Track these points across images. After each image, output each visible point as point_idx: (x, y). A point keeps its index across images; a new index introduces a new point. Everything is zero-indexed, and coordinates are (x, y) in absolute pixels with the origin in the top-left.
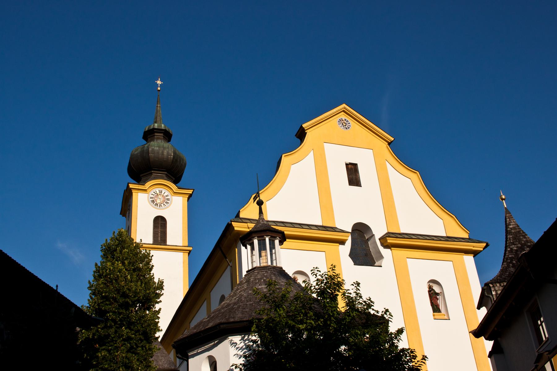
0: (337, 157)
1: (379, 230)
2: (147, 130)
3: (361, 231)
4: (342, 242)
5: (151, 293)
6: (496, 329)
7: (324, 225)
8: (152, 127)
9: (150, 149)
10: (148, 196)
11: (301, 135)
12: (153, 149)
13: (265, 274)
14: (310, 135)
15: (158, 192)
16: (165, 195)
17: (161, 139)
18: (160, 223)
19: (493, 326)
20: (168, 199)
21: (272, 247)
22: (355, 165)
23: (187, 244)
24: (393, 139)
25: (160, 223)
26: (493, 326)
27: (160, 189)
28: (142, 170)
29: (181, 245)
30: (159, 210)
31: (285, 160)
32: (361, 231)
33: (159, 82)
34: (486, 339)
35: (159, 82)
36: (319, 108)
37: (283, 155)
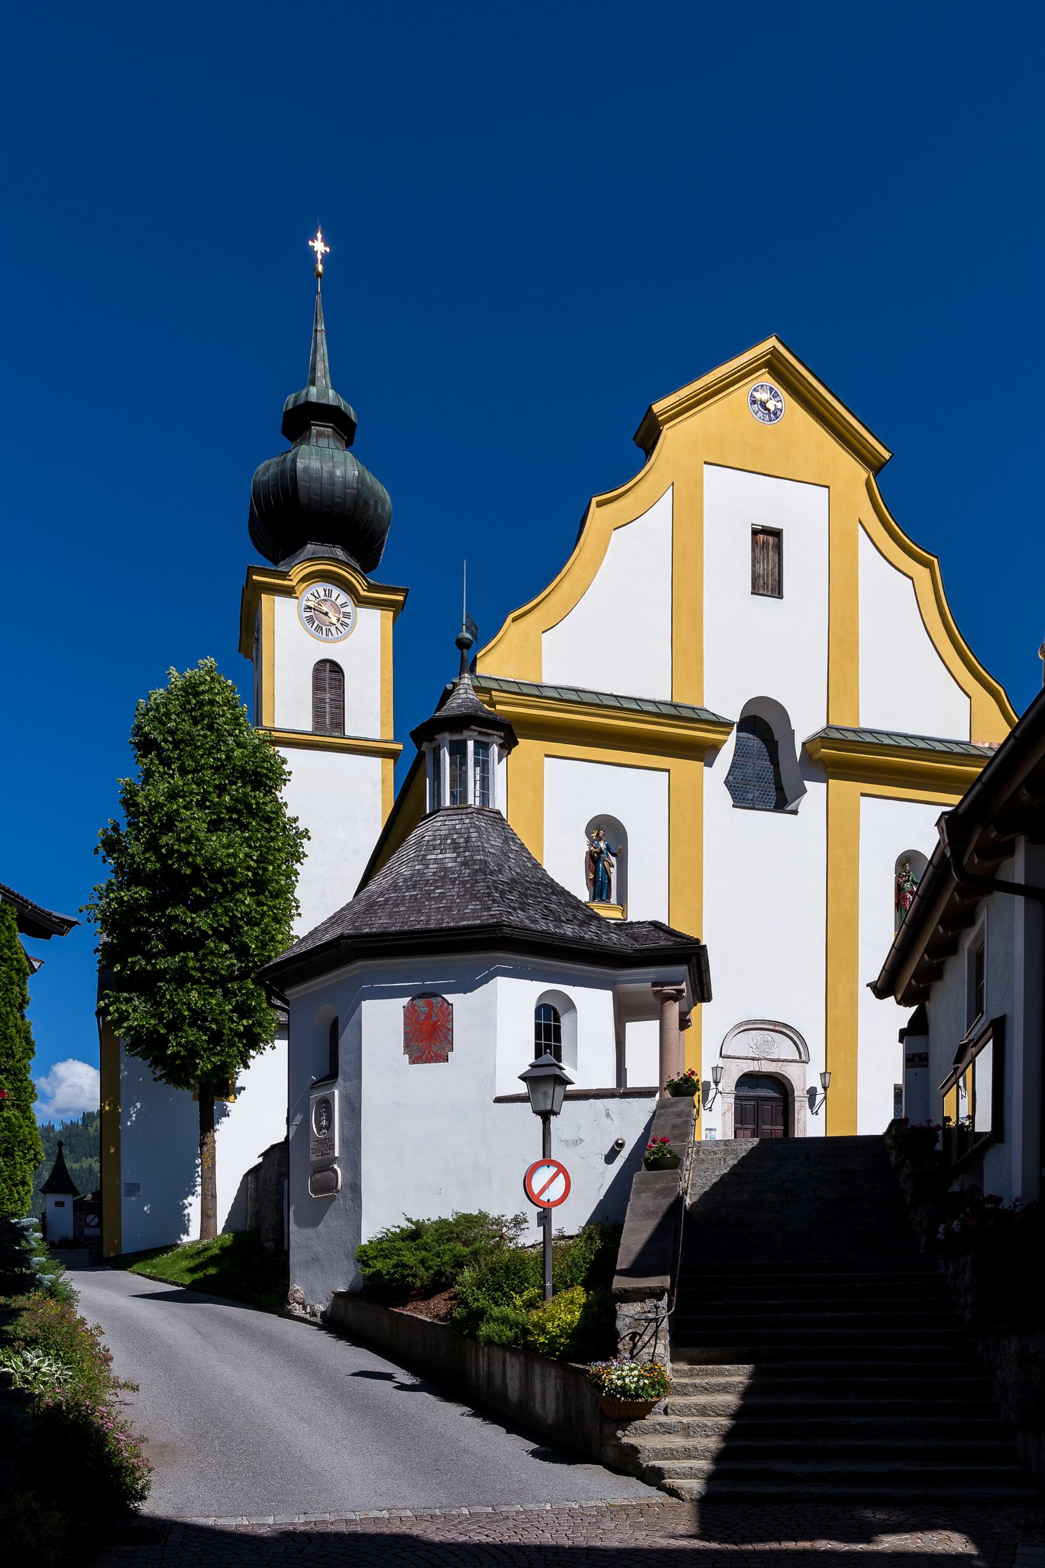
0: (734, 503)
1: (806, 724)
2: (290, 407)
3: (762, 723)
4: (705, 753)
5: (278, 846)
6: (913, 982)
7: (676, 701)
8: (302, 401)
9: (300, 465)
10: (299, 605)
11: (647, 437)
12: (306, 469)
13: (458, 827)
14: (670, 438)
15: (322, 594)
16: (339, 602)
17: (328, 437)
18: (329, 676)
19: (907, 978)
20: (347, 615)
21: (483, 765)
22: (777, 534)
23: (390, 736)
24: (887, 455)
25: (329, 676)
26: (907, 978)
27: (329, 586)
28: (291, 525)
29: (379, 738)
30: (323, 643)
31: (597, 517)
32: (762, 723)
33: (319, 246)
34: (899, 1003)
35: (319, 246)
36: (692, 353)
37: (594, 500)
